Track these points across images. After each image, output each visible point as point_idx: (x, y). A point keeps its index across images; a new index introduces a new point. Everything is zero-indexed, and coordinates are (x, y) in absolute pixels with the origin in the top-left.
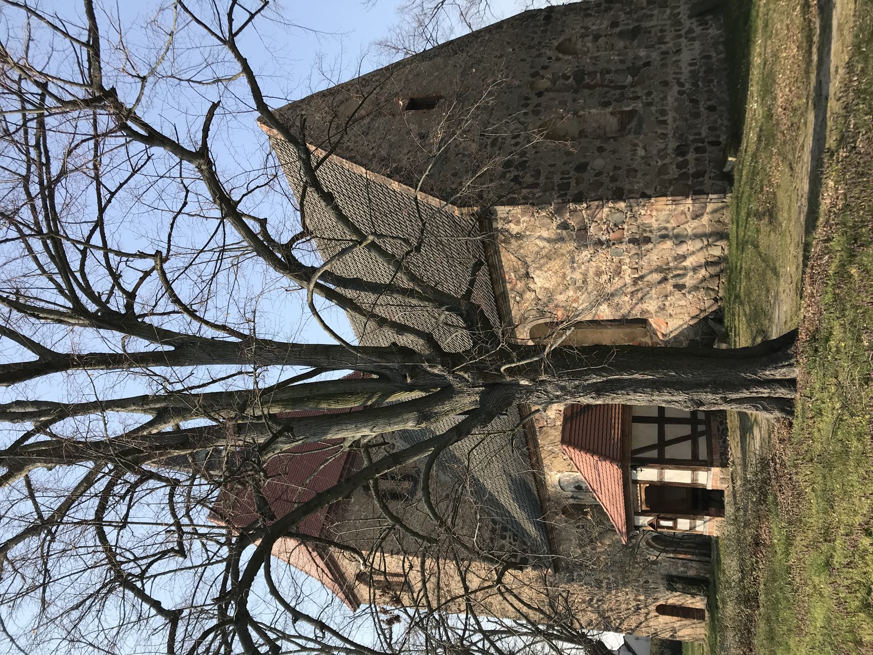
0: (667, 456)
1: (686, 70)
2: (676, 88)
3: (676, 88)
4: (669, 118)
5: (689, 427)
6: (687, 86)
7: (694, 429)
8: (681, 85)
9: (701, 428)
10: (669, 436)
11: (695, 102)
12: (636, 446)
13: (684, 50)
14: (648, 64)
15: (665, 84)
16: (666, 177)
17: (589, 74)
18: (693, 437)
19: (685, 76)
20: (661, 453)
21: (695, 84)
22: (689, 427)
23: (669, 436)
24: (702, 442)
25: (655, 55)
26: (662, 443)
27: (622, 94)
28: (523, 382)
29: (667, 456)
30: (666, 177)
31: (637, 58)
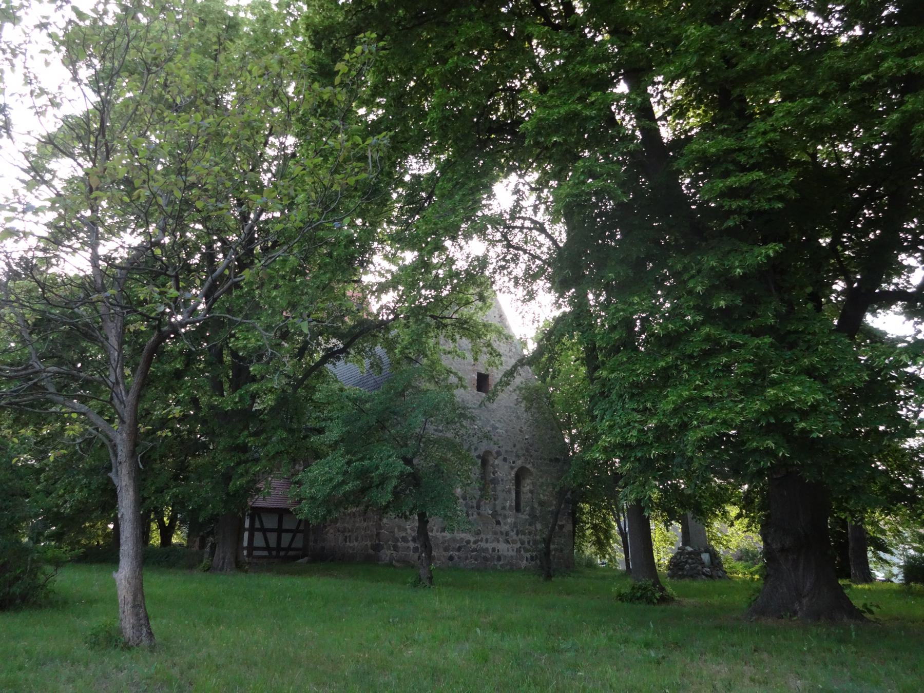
0: (256, 533)
1: (490, 546)
2: (472, 539)
3: (472, 539)
4: (447, 535)
5: (275, 546)
6: (475, 546)
7: (273, 549)
8: (475, 542)
9: (274, 553)
10: (269, 534)
11: (459, 549)
12: (262, 515)
13: (509, 546)
14: (498, 523)
15: (478, 533)
16: (396, 530)
17: (495, 487)
18: (267, 548)
19: (483, 545)
20: (258, 530)
21: (474, 550)
22: (275, 546)
23: (269, 534)
24: (265, 553)
25: (505, 528)
26: (264, 531)
27: (472, 507)
28: (87, 524)
29: (256, 533)
30: (396, 530)
31: (505, 517)
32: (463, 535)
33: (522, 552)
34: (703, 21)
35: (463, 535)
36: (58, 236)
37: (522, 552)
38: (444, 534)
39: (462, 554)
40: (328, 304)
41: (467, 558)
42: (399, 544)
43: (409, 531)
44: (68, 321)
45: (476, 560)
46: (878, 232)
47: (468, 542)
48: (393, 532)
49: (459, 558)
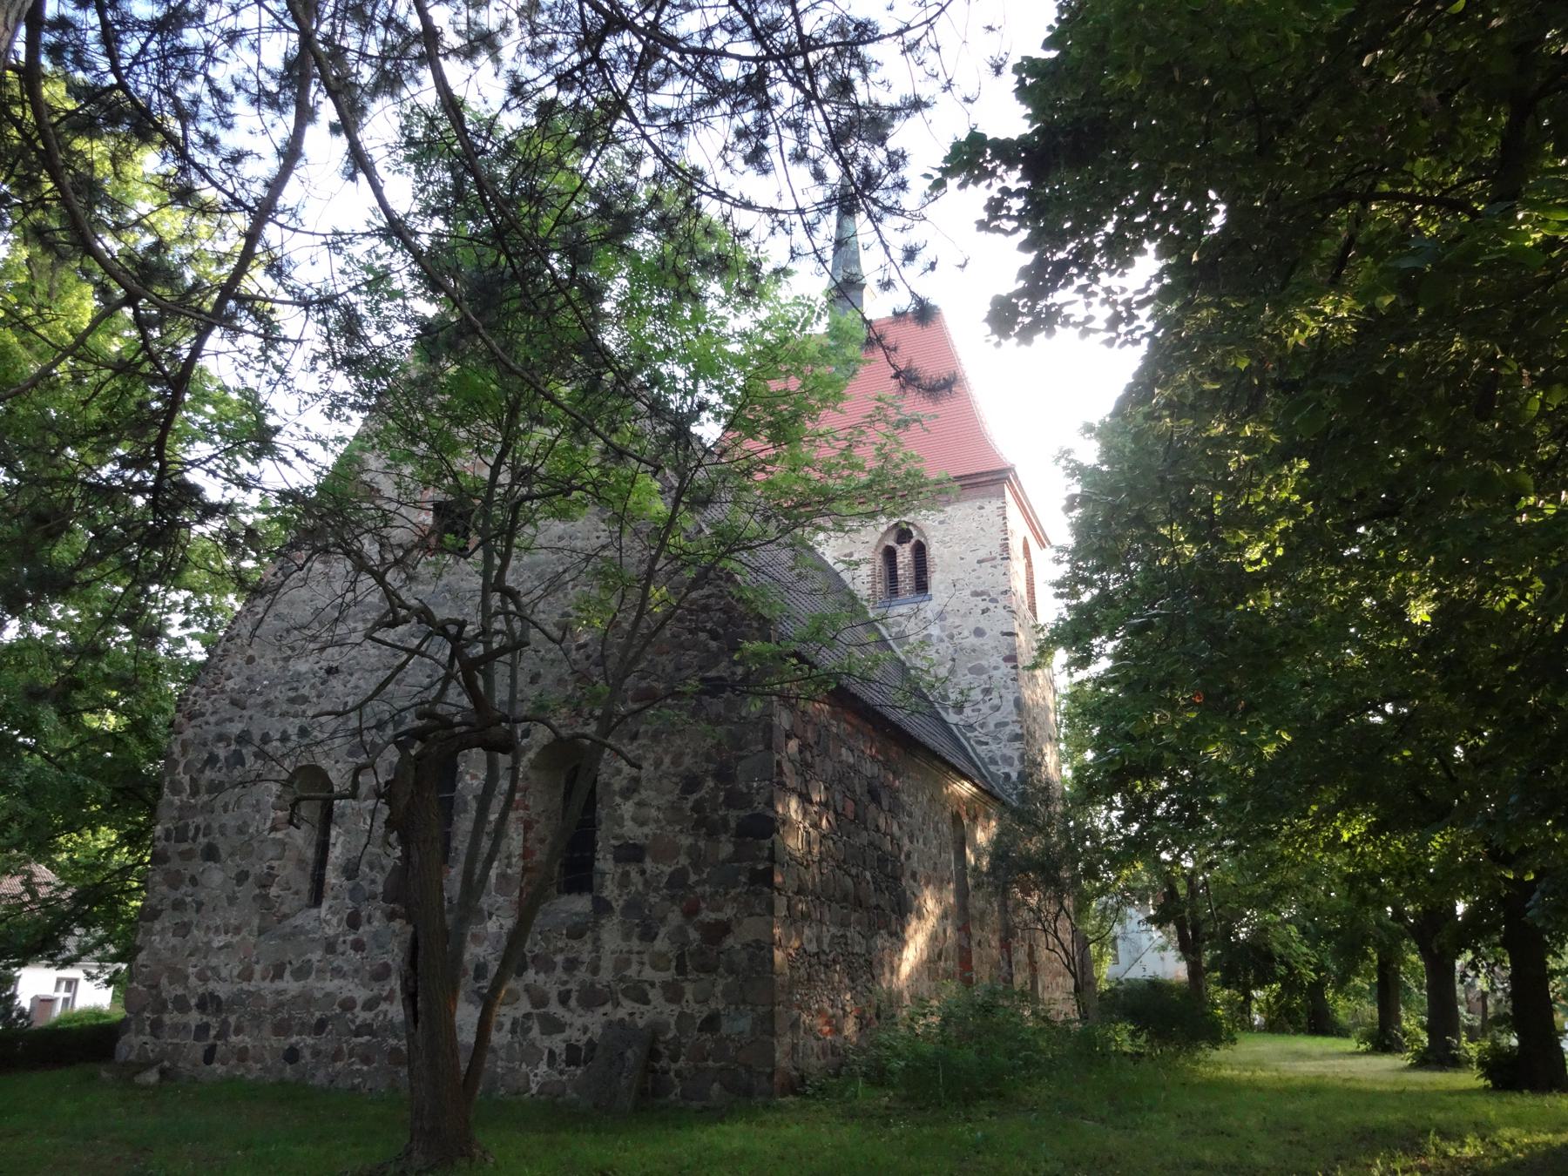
2: (361, 995)
4: (290, 985)
8: (370, 1005)
11: (320, 1026)
16: (164, 981)
21: (365, 1029)
32: (331, 985)
33: (535, 1032)
34: (36, 601)
35: (331, 985)
36: (474, 114)
37: (535, 1032)
38: (279, 985)
39: (326, 1043)
40: (1407, 264)
41: (337, 1056)
42: (167, 1018)
43: (193, 981)
44: (336, 853)
45: (366, 1060)
46: (1212, 195)
47: (348, 1005)
48: (156, 986)
49: (316, 1053)
